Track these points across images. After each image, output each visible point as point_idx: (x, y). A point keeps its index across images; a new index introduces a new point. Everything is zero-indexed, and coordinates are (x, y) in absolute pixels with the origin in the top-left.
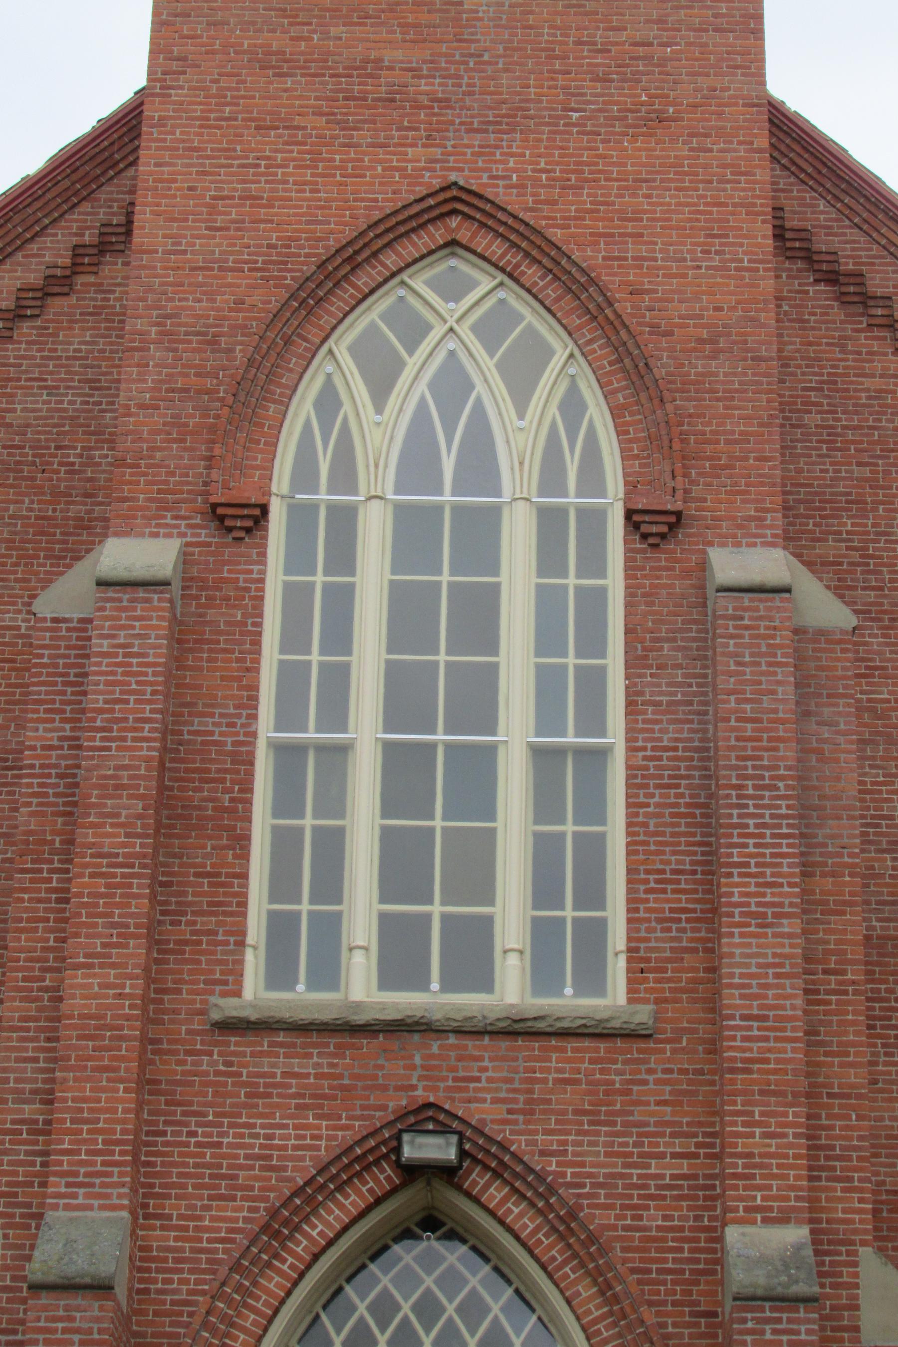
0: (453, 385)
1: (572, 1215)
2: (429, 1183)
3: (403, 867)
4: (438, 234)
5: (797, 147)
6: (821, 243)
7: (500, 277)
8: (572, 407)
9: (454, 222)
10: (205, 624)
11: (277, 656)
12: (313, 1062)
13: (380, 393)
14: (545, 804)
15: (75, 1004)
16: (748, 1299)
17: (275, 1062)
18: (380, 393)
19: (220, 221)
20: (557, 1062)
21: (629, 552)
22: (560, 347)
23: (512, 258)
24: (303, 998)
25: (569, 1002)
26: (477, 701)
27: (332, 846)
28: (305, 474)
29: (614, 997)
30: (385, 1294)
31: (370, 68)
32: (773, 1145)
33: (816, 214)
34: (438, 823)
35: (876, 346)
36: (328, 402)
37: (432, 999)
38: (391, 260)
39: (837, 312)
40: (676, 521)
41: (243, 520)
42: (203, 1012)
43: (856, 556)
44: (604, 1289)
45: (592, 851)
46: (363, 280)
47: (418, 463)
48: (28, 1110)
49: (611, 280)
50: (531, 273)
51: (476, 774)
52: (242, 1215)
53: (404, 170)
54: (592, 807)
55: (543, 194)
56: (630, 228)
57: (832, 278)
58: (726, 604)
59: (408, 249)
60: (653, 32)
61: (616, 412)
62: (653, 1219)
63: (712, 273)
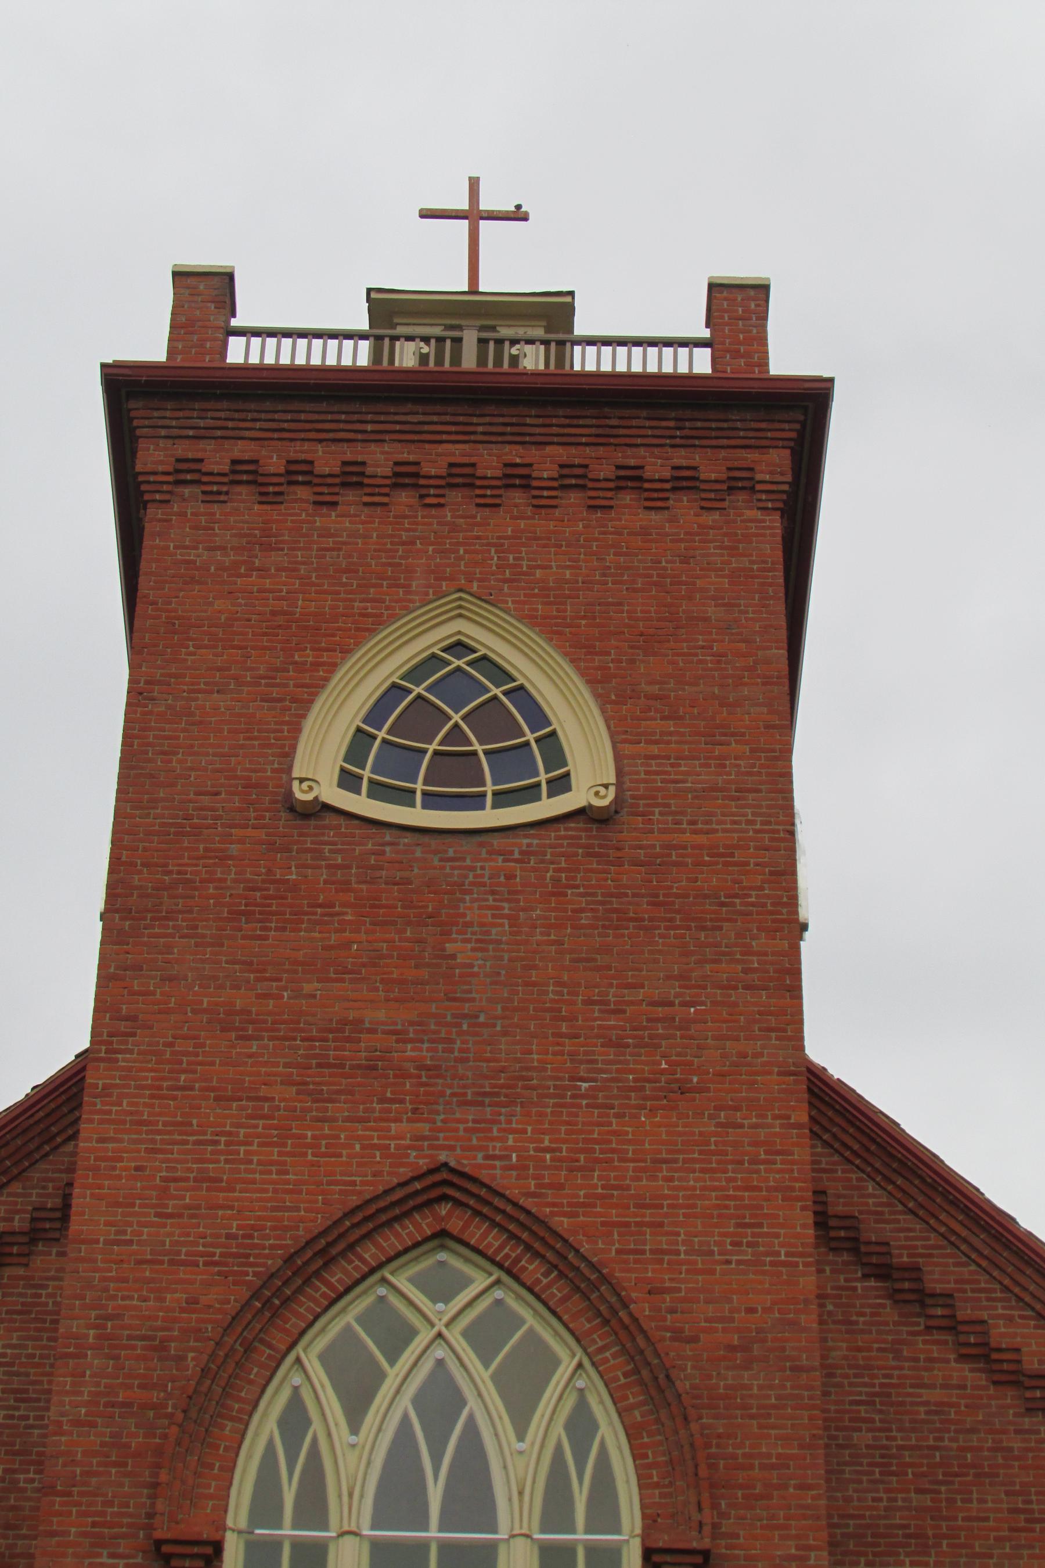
0: (440, 1400)
4: (425, 1223)
7: (497, 1274)
8: (581, 1426)
9: (444, 1209)
18: (356, 1407)
22: (567, 1356)
28: (266, 1507)
33: (865, 1198)
35: (935, 1352)
36: (296, 1419)
38: (369, 1253)
39: (890, 1312)
46: (337, 1277)
50: (533, 1268)
56: (648, 1216)
59: (390, 1242)
61: (632, 1432)
63: (744, 1269)
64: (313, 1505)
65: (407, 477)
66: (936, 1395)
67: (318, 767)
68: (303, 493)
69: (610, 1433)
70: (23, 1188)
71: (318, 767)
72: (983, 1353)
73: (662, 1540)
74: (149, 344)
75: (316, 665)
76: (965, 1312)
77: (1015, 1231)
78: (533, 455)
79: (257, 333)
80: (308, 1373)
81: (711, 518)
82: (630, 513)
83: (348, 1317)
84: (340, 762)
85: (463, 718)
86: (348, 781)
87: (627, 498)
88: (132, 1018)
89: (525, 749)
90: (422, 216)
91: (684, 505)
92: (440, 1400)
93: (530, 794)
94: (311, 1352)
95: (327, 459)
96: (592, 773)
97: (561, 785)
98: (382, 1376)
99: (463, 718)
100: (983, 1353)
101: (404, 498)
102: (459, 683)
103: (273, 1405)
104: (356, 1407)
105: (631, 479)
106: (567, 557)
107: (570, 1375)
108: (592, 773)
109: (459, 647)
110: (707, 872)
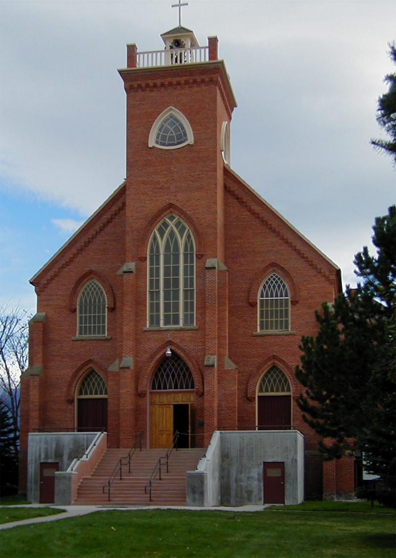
0: (172, 234)
1: (136, 436)
3: (167, 308)
6: (236, 193)
8: (189, 237)
9: (171, 209)
10: (140, 271)
11: (183, 223)
13: (162, 237)
14: (186, 297)
18: (162, 237)
19: (138, 211)
20: (186, 334)
21: (196, 260)
22: (188, 228)
31: (158, 183)
32: (212, 345)
34: (172, 301)
35: (245, 210)
36: (155, 238)
39: (239, 205)
40: (202, 256)
42: (142, 329)
43: (239, 246)
47: (167, 247)
52: (147, 355)
53: (162, 200)
54: (192, 298)
55: (184, 203)
56: (197, 208)
57: (238, 199)
60: (200, 173)
62: (199, 354)
65: (163, 85)
67: (152, 143)
68: (148, 89)
71: (152, 143)
72: (250, 210)
74: (124, 66)
75: (152, 121)
76: (248, 205)
77: (161, 329)
78: (181, 79)
79: (141, 53)
81: (207, 88)
82: (196, 89)
83: (160, 224)
84: (190, 449)
85: (173, 276)
86: (157, 142)
88: (131, 183)
89: (182, 137)
91: (203, 85)
95: (151, 83)
98: (165, 232)
99: (173, 315)
100: (250, 210)
101: (163, 88)
102: (172, 121)
105: (195, 82)
108: (191, 140)
110: (207, 150)
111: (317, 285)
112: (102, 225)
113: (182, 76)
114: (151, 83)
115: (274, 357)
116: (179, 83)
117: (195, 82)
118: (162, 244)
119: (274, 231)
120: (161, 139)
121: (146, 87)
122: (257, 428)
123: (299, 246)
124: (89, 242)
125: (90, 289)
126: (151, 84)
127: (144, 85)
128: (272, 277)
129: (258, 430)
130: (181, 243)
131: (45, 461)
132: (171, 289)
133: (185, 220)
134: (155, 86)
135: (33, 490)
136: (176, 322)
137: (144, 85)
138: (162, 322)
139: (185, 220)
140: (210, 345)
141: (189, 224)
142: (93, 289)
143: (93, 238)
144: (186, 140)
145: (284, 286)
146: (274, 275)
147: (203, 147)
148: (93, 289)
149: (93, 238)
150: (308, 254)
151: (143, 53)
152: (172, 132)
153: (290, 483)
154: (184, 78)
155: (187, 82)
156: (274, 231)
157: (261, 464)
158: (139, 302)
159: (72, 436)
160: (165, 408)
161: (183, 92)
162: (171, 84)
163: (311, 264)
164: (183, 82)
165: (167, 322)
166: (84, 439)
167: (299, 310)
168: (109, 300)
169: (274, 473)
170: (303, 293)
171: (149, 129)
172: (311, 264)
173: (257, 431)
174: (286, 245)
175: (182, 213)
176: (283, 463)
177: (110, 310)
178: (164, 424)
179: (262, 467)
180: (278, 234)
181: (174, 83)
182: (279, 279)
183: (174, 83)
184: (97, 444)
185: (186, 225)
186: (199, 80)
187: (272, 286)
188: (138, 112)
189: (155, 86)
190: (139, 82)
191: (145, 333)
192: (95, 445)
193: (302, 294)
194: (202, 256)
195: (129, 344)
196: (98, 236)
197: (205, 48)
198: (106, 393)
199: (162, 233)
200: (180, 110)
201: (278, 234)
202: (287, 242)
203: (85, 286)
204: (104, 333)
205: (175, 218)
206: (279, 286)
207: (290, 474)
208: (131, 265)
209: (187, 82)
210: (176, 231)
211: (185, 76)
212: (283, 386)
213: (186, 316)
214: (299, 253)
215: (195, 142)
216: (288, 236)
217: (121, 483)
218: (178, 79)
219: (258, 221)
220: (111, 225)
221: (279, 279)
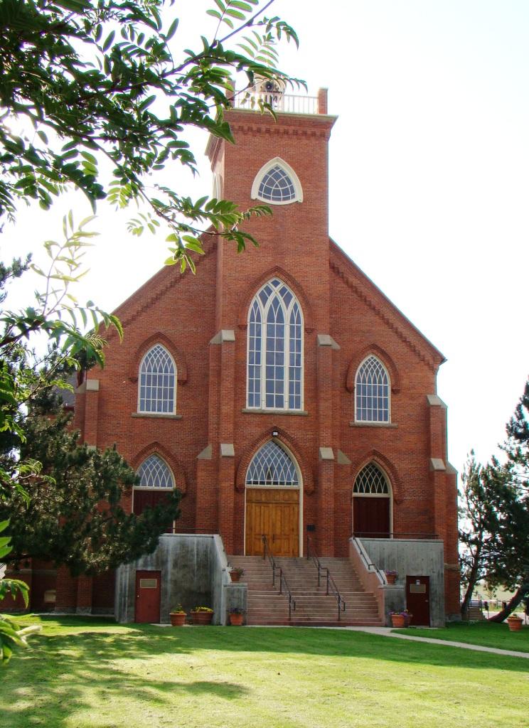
0: (276, 302)
2: (477, 585)
3: (269, 387)
5: (333, 247)
10: (239, 344)
12: (257, 419)
15: (224, 411)
16: (224, 457)
17: (251, 419)
18: (264, 302)
20: (293, 420)
22: (294, 297)
23: (286, 280)
24: (254, 408)
25: (295, 410)
26: (280, 359)
27: (258, 383)
28: (252, 319)
29: (302, 409)
30: (282, 459)
33: (337, 263)
36: (256, 304)
37: (274, 409)
40: (312, 330)
41: (242, 328)
44: (301, 455)
45: (298, 385)
48: (215, 426)
49: (302, 284)
50: (289, 282)
51: (280, 371)
54: (298, 378)
58: (321, 347)
60: (310, 235)
61: (303, 309)
63: (319, 281)
64: (259, 320)
66: (340, 289)
67: (254, 195)
69: (300, 308)
70: (92, 613)
72: (347, 282)
73: (307, 327)
80: (257, 298)
86: (260, 194)
87: (304, 137)
89: (288, 192)
90: (202, 37)
91: (313, 139)
92: (276, 302)
93: (288, 198)
94: (258, 294)
95: (255, 127)
96: (299, 196)
97: (293, 197)
100: (347, 282)
103: (253, 302)
104: (264, 302)
105: (305, 133)
106: (393, 684)
107: (294, 300)
108: (299, 196)
109: (277, 168)
110: (314, 211)
111: (420, 374)
112: (173, 280)
113: (290, 126)
114: (255, 127)
115: (375, 453)
116: (286, 132)
117: (305, 133)
118: (264, 312)
119: (374, 309)
120: (265, 190)
121: (239, 130)
122: (174, 530)
123: (401, 328)
124: (157, 299)
125: (155, 356)
126: (255, 128)
127: (246, 128)
128: (155, 349)
129: (176, 533)
130: (287, 314)
131: (144, 569)
132: (275, 365)
133: (293, 287)
134: (259, 131)
135: (127, 606)
136: (280, 404)
137: (246, 128)
138: (286, 404)
139: (293, 287)
140: (324, 435)
141: (297, 292)
142: (164, 356)
143: (161, 294)
144: (293, 197)
145: (383, 372)
146: (372, 358)
147: (312, 207)
148: (164, 356)
149: (161, 294)
150: (411, 338)
151: (289, 96)
152: (277, 185)
153: (437, 602)
154: (293, 128)
155: (296, 133)
156: (374, 309)
157: (403, 579)
158: (239, 379)
159: (179, 539)
160: (262, 507)
161: (290, 142)
162: (277, 132)
163: (413, 349)
164: (291, 132)
165: (269, 403)
166: (194, 543)
167: (400, 400)
168: (181, 371)
169: (418, 588)
170: (405, 382)
171: (253, 179)
172: (413, 349)
173: (392, 539)
174: (386, 326)
175: (289, 279)
176: (428, 577)
177: (182, 383)
178: (262, 526)
179: (405, 581)
180: (378, 313)
181: (281, 131)
182: (378, 363)
183: (281, 131)
184: (361, 556)
185: (292, 293)
186: (309, 132)
187: (369, 370)
188: (238, 157)
189: (259, 131)
190: (240, 124)
191: (245, 416)
192: (361, 553)
193: (403, 382)
194: (312, 330)
195: (227, 427)
196: (168, 293)
197: (314, 98)
198: (386, 491)
199: (264, 300)
200: (288, 162)
201: (378, 313)
202: (387, 323)
203: (150, 352)
204: (171, 410)
205: (279, 283)
206: (377, 372)
207: (436, 591)
208: (228, 335)
209: (296, 133)
210: (281, 299)
211: (294, 125)
212: (163, 481)
213: (291, 398)
214: (400, 336)
215: (304, 201)
216: (389, 316)
217: (328, 599)
218: (286, 128)
219: (355, 295)
220: (183, 281)
221: (378, 363)
